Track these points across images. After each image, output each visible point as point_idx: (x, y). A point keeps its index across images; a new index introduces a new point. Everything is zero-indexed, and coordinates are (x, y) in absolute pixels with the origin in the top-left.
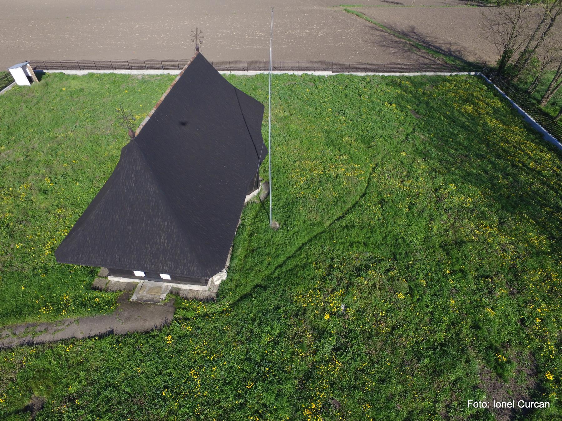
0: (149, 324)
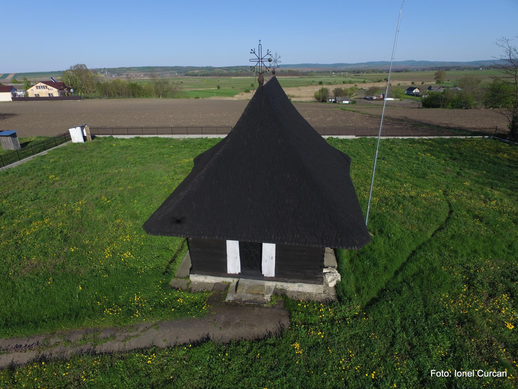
0: (260, 330)
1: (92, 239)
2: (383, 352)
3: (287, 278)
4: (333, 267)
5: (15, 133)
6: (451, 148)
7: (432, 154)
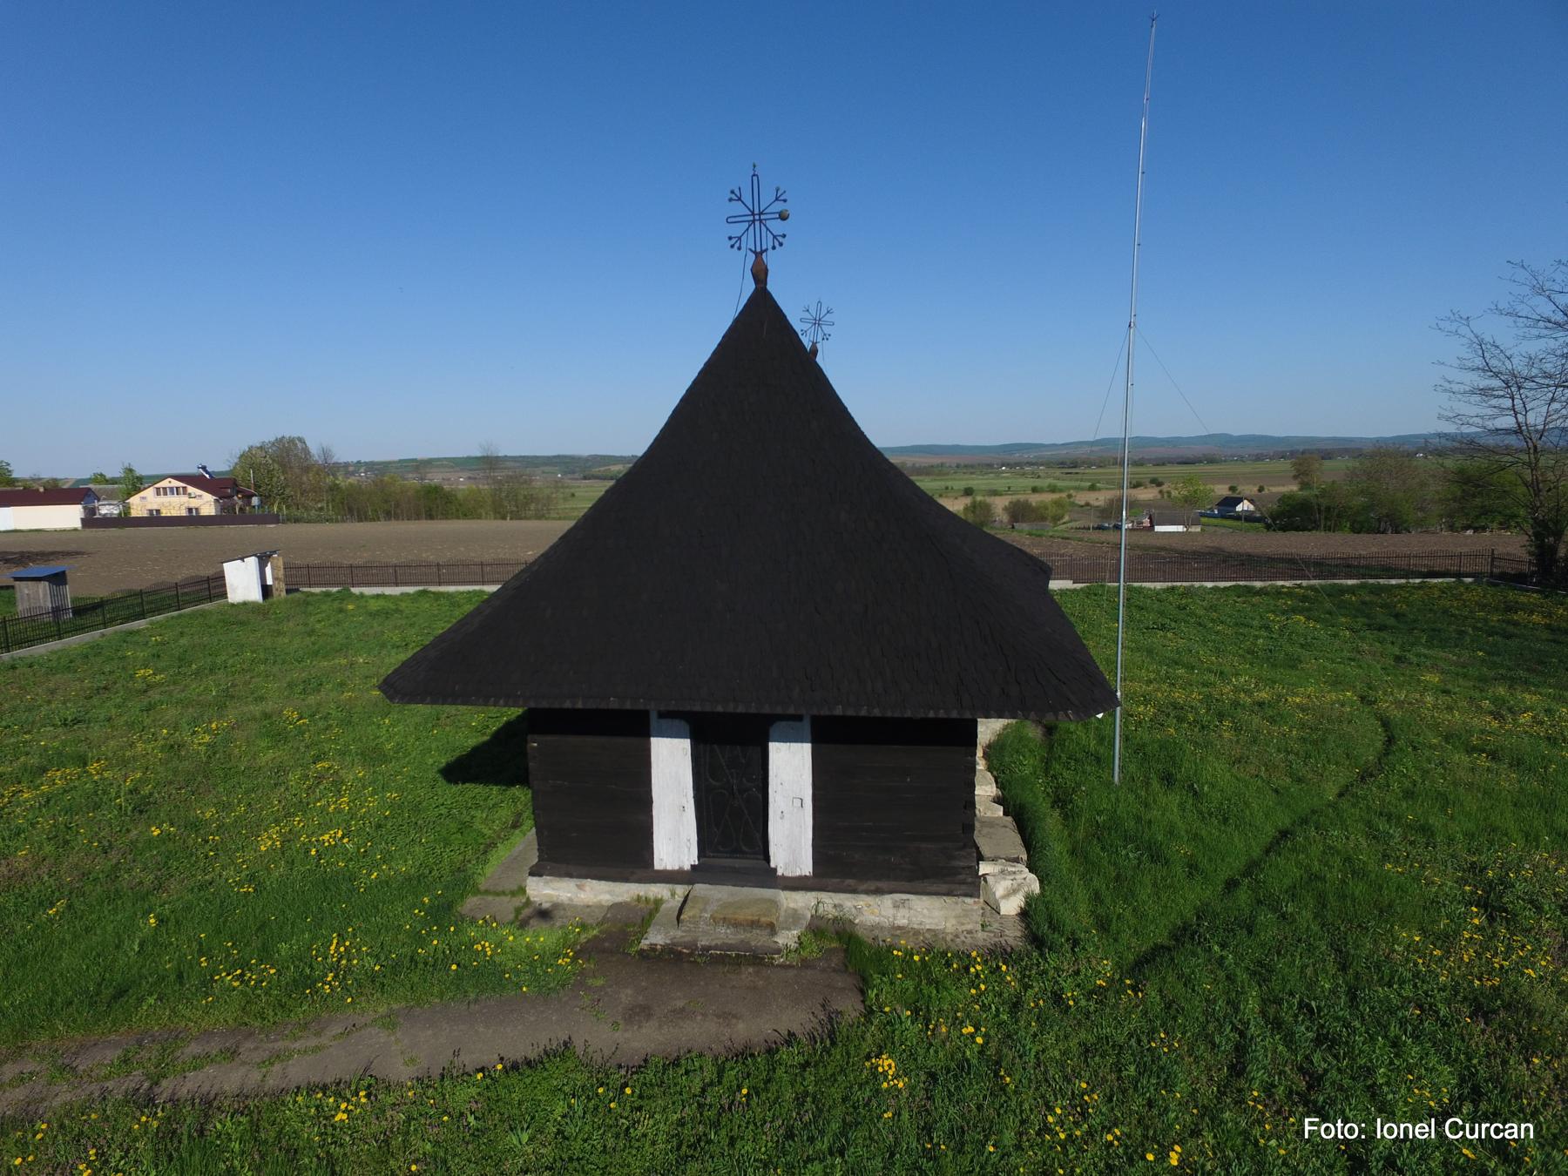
0: (753, 1028)
1: (226, 807)
2: (1209, 1092)
3: (853, 876)
4: (1017, 860)
5: (64, 573)
6: (1364, 603)
7: (1308, 618)
